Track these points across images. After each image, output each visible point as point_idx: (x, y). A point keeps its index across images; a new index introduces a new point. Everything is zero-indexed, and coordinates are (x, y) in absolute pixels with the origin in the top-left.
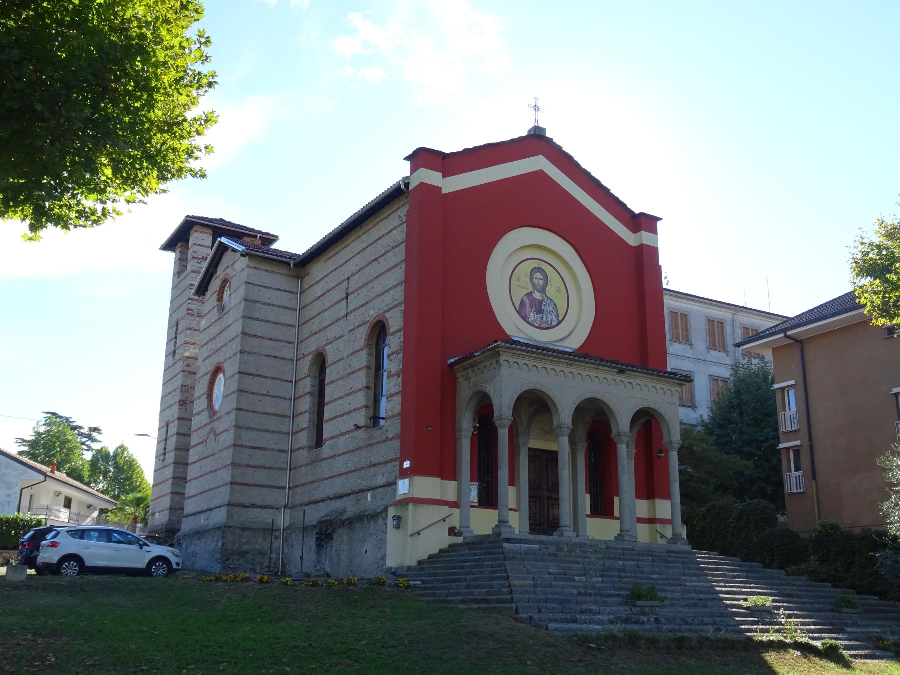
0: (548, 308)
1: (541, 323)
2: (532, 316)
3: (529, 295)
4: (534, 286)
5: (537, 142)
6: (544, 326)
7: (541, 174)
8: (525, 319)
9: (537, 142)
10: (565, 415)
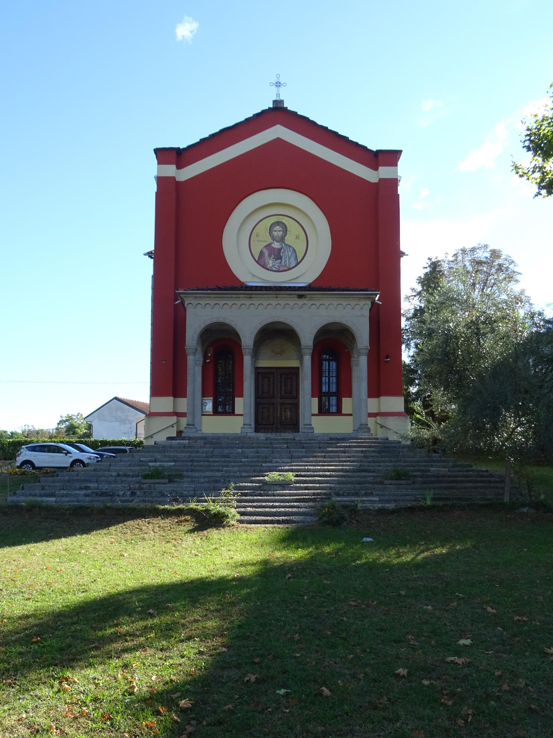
0: (286, 254)
1: (279, 267)
2: (270, 263)
3: (268, 246)
4: (273, 238)
5: (278, 113)
6: (282, 269)
7: (278, 142)
8: (264, 266)
9: (278, 113)
10: (307, 339)
